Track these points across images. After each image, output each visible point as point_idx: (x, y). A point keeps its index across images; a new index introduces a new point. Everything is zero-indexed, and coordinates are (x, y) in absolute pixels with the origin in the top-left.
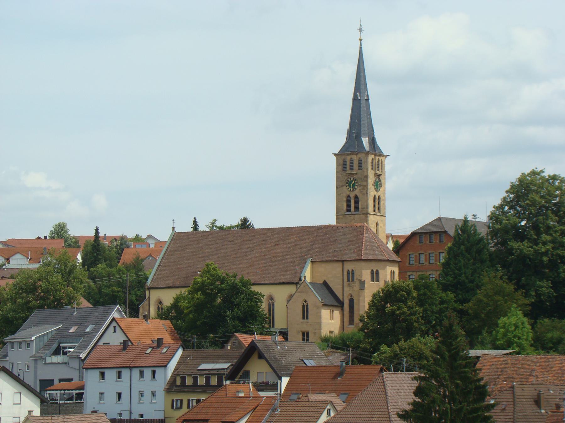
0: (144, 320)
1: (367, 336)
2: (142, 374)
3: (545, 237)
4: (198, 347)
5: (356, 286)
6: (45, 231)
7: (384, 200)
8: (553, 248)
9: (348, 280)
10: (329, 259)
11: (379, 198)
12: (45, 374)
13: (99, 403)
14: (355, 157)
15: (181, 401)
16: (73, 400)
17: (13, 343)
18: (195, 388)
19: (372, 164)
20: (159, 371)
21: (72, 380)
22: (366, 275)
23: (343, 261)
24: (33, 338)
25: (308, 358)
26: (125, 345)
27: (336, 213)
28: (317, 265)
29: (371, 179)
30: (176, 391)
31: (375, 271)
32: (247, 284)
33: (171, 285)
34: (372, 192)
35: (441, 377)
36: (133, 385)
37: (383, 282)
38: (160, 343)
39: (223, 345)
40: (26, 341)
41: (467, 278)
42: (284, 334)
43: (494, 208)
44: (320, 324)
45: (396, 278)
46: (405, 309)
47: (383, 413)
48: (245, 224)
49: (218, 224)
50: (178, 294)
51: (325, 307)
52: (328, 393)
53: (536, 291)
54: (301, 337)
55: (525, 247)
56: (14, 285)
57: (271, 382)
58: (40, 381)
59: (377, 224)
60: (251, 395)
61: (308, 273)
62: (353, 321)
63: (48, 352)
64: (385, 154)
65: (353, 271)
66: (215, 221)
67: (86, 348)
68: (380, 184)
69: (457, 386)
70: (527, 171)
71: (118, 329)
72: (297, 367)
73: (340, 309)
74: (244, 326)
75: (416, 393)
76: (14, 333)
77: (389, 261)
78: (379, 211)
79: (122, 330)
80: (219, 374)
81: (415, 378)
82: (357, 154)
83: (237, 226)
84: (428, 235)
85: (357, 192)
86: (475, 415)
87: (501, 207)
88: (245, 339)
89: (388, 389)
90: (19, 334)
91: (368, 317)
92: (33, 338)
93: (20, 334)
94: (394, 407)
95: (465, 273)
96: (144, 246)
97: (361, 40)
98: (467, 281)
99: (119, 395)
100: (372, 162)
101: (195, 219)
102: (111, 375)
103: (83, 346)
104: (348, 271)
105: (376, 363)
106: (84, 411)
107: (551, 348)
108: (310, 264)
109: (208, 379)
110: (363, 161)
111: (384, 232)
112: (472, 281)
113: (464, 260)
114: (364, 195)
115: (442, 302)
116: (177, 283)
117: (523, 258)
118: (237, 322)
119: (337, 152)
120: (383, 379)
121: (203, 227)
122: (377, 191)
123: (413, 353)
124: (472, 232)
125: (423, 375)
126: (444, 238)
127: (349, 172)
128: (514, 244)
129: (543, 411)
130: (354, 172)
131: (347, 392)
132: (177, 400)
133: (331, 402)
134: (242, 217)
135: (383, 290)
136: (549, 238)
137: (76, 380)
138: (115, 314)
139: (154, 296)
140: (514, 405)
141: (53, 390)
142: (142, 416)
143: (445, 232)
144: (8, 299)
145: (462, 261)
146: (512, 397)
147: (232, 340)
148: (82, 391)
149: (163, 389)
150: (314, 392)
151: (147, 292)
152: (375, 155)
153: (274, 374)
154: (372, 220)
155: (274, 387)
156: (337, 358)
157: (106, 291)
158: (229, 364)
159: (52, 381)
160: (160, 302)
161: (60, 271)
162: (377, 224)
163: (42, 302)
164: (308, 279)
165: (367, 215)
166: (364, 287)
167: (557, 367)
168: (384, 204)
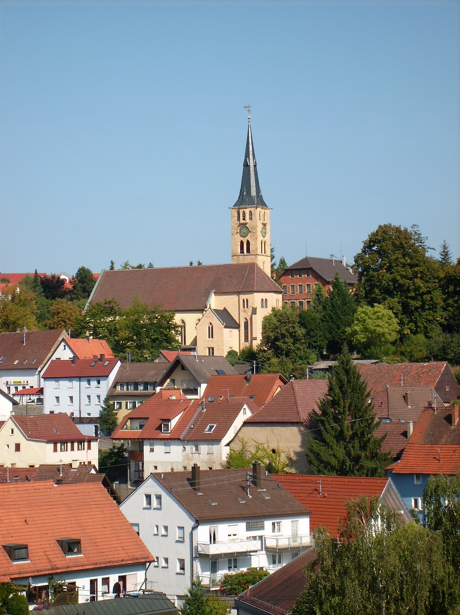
34: (260, 238)
36: (81, 390)
84: (298, 271)
99: (71, 398)
108: (213, 294)
121: (117, 267)
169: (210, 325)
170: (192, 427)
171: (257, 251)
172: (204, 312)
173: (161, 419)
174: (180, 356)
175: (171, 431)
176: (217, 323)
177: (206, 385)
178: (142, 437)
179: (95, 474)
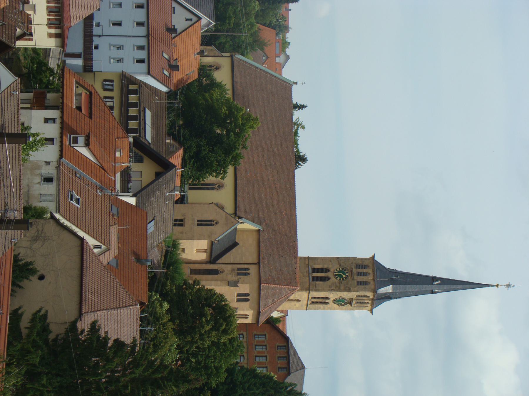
0: (198, 51)
1: (179, 288)
5: (232, 278)
7: (324, 309)
11: (327, 303)
14: (370, 278)
15: (112, 90)
18: (126, 105)
19: (362, 296)
20: (144, 66)
22: (244, 288)
23: (259, 263)
25: (156, 225)
26: (172, 30)
28: (255, 235)
29: (346, 295)
31: (248, 297)
32: (235, 160)
34: (333, 296)
36: (129, 39)
38: (175, 68)
39: (171, 134)
44: (192, 238)
45: (240, 321)
46: (207, 328)
48: (301, 159)
49: (300, 131)
52: (119, 247)
57: (131, 185)
59: (298, 301)
60: (117, 165)
61: (246, 226)
62: (195, 274)
64: (374, 310)
65: (249, 274)
66: (303, 127)
69: (125, 387)
71: (190, 23)
72: (147, 213)
73: (208, 260)
74: (191, 158)
77: (259, 312)
78: (312, 303)
80: (140, 131)
82: (374, 280)
83: (298, 151)
84: (286, 355)
85: (333, 280)
88: (176, 159)
91: (199, 289)
96: (277, 52)
97: (497, 286)
99: (119, 24)
100: (365, 296)
101: (306, 106)
102: (141, 15)
104: (248, 269)
105: (150, 297)
109: (134, 118)
110: (366, 286)
111: (290, 308)
116: (238, 87)
118: (195, 149)
119: (376, 259)
120: (132, 305)
121: (297, 115)
122: (335, 301)
126: (283, 372)
127: (355, 271)
130: (355, 277)
131: (119, 267)
132: (112, 85)
133: (108, 250)
134: (307, 156)
138: (205, 20)
139: (224, 62)
142: (97, 48)
143: (289, 374)
147: (176, 144)
152: (373, 300)
153: (140, 189)
154: (303, 296)
155: (125, 189)
158: (150, 140)
160: (217, 68)
162: (298, 301)
164: (240, 226)
165: (308, 290)
169: (215, 222)
170: (78, 175)
171: (315, 291)
172: (233, 216)
173: (89, 133)
174: (174, 169)
175: (73, 147)
178: (65, 108)
179: (15, 34)
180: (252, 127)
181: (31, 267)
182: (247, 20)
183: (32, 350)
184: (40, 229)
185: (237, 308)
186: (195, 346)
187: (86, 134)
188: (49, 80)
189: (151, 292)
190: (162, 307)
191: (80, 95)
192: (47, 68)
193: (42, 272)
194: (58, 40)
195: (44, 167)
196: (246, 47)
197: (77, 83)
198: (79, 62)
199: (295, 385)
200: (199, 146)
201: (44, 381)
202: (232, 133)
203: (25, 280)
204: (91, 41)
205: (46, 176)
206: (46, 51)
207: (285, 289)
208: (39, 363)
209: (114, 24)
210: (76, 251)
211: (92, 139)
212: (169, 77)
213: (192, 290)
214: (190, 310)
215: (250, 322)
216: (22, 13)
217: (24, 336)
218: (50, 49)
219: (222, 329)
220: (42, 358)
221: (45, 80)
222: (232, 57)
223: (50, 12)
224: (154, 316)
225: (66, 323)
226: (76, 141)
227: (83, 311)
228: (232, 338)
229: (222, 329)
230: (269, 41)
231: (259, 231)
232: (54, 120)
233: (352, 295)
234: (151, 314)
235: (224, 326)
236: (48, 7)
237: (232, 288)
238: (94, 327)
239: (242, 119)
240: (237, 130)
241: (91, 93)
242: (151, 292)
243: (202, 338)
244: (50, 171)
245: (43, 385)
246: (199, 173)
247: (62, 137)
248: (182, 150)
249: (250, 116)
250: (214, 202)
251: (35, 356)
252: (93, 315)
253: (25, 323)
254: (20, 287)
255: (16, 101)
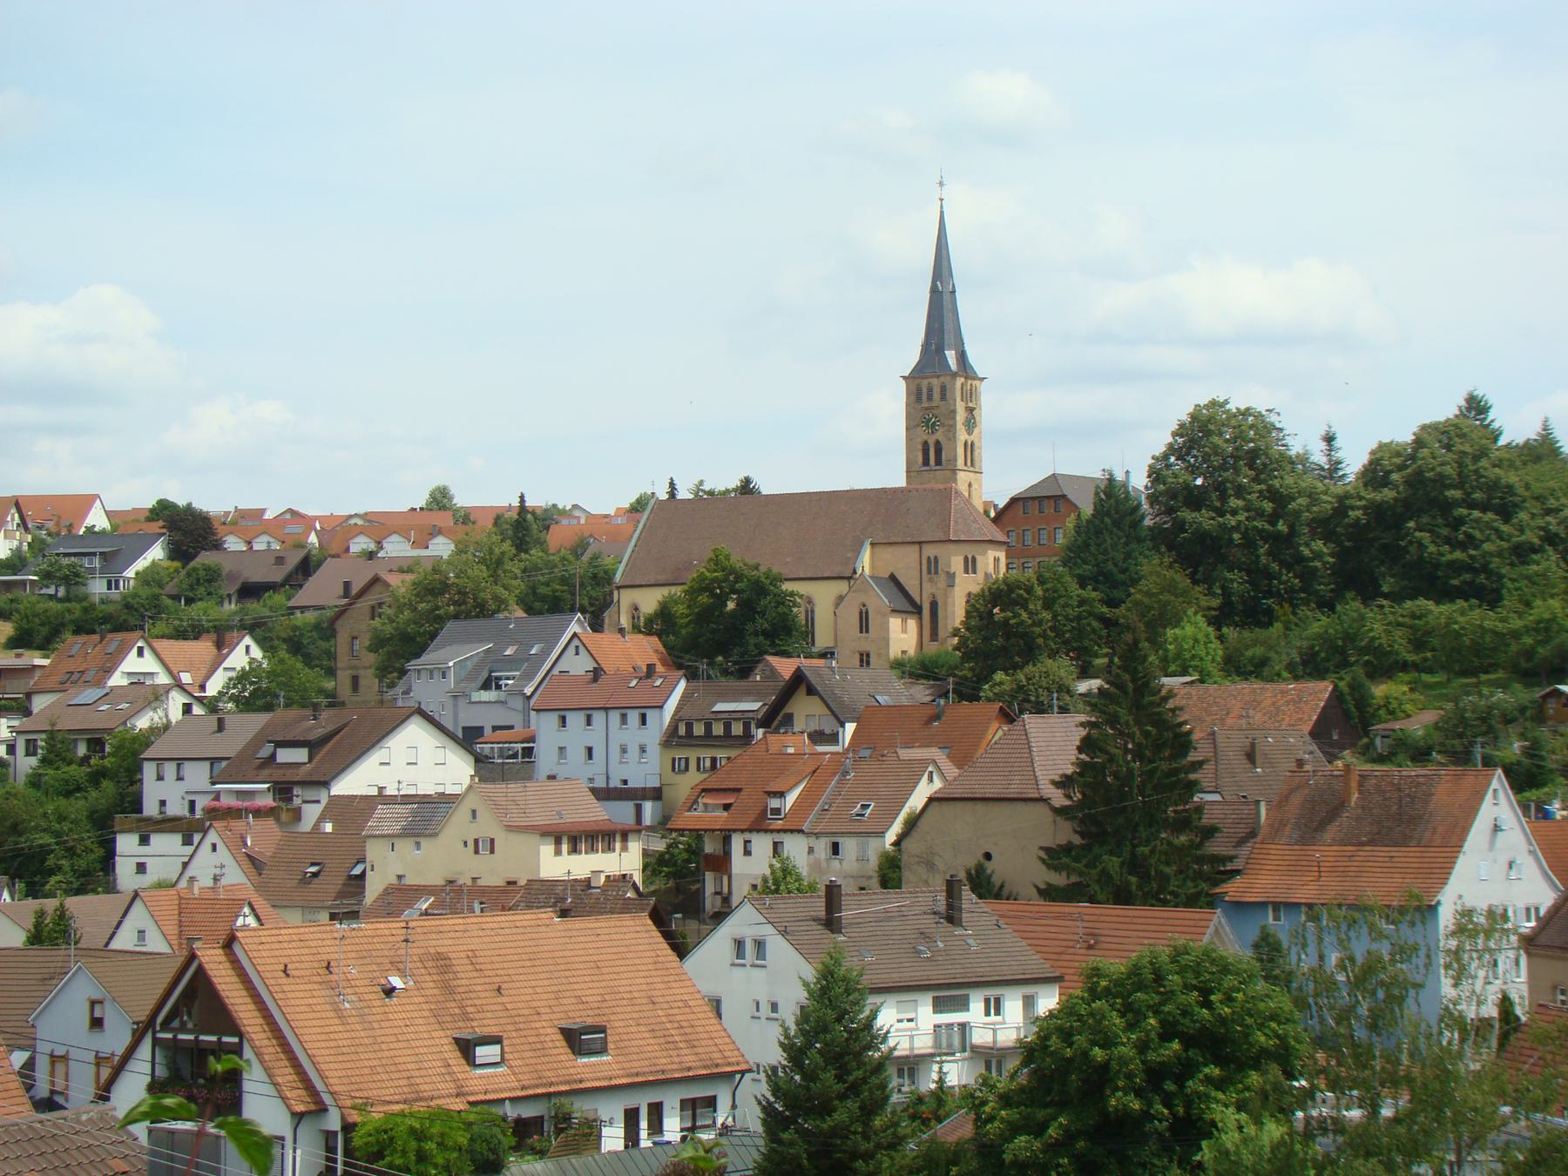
0: (619, 636)
1: (966, 657)
2: (624, 718)
3: (1234, 503)
4: (335, 659)
5: (941, 581)
6: (421, 501)
7: (980, 448)
8: (1247, 519)
9: (929, 572)
10: (900, 540)
12: (470, 718)
13: (559, 763)
14: (935, 382)
15: (687, 760)
16: (517, 758)
17: (419, 671)
18: (708, 739)
19: (962, 393)
21: (511, 727)
22: (957, 564)
23: (920, 543)
24: (451, 664)
25: (881, 694)
26: (597, 673)
27: (907, 468)
28: (879, 549)
29: (961, 416)
30: (679, 745)
31: (970, 557)
33: (652, 582)
34: (962, 436)
35: (1122, 721)
36: (610, 735)
37: (983, 574)
39: (744, 672)
40: (439, 669)
41: (1116, 565)
42: (826, 654)
43: (1153, 458)
44: (886, 641)
45: (1003, 569)
46: (1024, 615)
47: (1026, 777)
48: (746, 487)
49: (707, 487)
50: (666, 594)
51: (895, 614)
52: (919, 746)
53: (1223, 588)
54: (872, 660)
55: (1204, 519)
56: (414, 584)
57: (828, 731)
58: (464, 728)
59: (970, 485)
60: (807, 751)
61: (865, 561)
62: (937, 635)
63: (473, 685)
64: (980, 376)
65: (936, 557)
66: (701, 483)
67: (532, 679)
68: (974, 423)
69: (1146, 734)
70: (1203, 401)
71: (582, 649)
72: (867, 707)
73: (916, 616)
74: (773, 644)
75: (1080, 749)
76: (418, 656)
77: (991, 542)
78: (972, 465)
79: (589, 651)
80: (746, 719)
81: (1082, 724)
82: (938, 377)
83: (735, 490)
84: (1037, 502)
85: (939, 435)
86: (1174, 779)
87: (1165, 457)
88: (785, 667)
89: (1032, 740)
90: (425, 658)
91: (968, 629)
92: (451, 664)
93: (428, 658)
94: (1043, 768)
95: (1113, 559)
97: (941, 200)
98: (1115, 570)
99: (590, 750)
100: (962, 389)
101: (672, 479)
102: (576, 719)
103: (528, 676)
104: (929, 558)
105: (989, 700)
106: (536, 776)
107: (1251, 673)
109: (727, 726)
110: (948, 386)
111: (981, 497)
112: (1124, 571)
113: (1112, 539)
114: (950, 439)
115: (1082, 602)
116: (662, 578)
117: (1202, 537)
118: (761, 638)
119: (907, 375)
120: (1024, 725)
121: (684, 494)
122: (970, 432)
123: (1048, 683)
124: (1123, 496)
125: (1093, 719)
126: (1061, 506)
127: (925, 405)
128: (1187, 515)
129: (1259, 770)
131: (949, 745)
132: (680, 759)
133: (934, 762)
134: (742, 477)
135: (990, 589)
136: (1240, 503)
137: (519, 728)
138: (574, 627)
139: (626, 598)
140: (1216, 762)
141: (486, 743)
142: (625, 782)
143: (1064, 496)
144: (405, 604)
145: (1109, 541)
146: (1212, 750)
147: (760, 666)
148: (531, 745)
149: (658, 742)
150: (908, 745)
151: (616, 593)
152: (966, 378)
153: (832, 717)
154: (963, 478)
155: (833, 738)
156: (921, 693)
157: (543, 590)
158: (759, 704)
159: (481, 729)
160: (636, 609)
161: (483, 561)
162: (970, 485)
163: (457, 608)
164: (867, 571)
165: (954, 471)
166: (954, 582)
167: (1268, 702)
168: (980, 454)
170: (826, 808)
173: (765, 792)
176: (879, 599)
177: (854, 725)
180: (727, 558)
181: (973, 872)
182: (556, 566)
183: (1100, 868)
184: (917, 859)
185: (986, 573)
186: (1049, 632)
187: (766, 796)
188: (685, 850)
189: (980, 698)
190: (1001, 683)
191: (706, 805)
192: (667, 853)
193: (980, 856)
194: (630, 837)
195: (816, 855)
196: (596, 567)
197: (689, 810)
198: (648, 807)
199: (1097, 487)
200: (756, 634)
201: (1146, 850)
202: (737, 586)
203: (992, 880)
204: (616, 789)
205: (830, 851)
206: (645, 853)
207: (955, 505)
208: (1119, 857)
209: (590, 756)
210: (948, 808)
211: (773, 787)
212: (665, 677)
213: (968, 639)
214: (998, 642)
215: (1004, 554)
216: (604, 889)
217: (1078, 880)
218: (643, 849)
219: (1025, 595)
220: (1111, 853)
221: (685, 856)
222: (618, 588)
223: (609, 849)
224: (1016, 692)
225: (1055, 821)
226: (777, 811)
227: (1036, 796)
228: (1038, 580)
229: (1025, 595)
230: (576, 534)
231: (872, 544)
232: (747, 842)
233: (960, 407)
234: (1014, 697)
235: (1021, 592)
236: (586, 853)
237: (957, 581)
238: (1064, 783)
239: (715, 571)
240: (731, 578)
241: (704, 790)
242: (980, 698)
243: (1039, 623)
244: (822, 846)
245: (1152, 852)
246: (794, 633)
247: (772, 831)
248: (770, 658)
249: (711, 559)
250: (832, 609)
251: (1111, 864)
252: (1042, 782)
253: (1059, 879)
254: (1002, 886)
255: (779, 901)
